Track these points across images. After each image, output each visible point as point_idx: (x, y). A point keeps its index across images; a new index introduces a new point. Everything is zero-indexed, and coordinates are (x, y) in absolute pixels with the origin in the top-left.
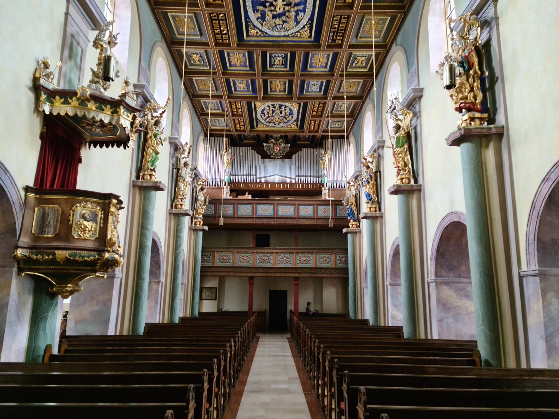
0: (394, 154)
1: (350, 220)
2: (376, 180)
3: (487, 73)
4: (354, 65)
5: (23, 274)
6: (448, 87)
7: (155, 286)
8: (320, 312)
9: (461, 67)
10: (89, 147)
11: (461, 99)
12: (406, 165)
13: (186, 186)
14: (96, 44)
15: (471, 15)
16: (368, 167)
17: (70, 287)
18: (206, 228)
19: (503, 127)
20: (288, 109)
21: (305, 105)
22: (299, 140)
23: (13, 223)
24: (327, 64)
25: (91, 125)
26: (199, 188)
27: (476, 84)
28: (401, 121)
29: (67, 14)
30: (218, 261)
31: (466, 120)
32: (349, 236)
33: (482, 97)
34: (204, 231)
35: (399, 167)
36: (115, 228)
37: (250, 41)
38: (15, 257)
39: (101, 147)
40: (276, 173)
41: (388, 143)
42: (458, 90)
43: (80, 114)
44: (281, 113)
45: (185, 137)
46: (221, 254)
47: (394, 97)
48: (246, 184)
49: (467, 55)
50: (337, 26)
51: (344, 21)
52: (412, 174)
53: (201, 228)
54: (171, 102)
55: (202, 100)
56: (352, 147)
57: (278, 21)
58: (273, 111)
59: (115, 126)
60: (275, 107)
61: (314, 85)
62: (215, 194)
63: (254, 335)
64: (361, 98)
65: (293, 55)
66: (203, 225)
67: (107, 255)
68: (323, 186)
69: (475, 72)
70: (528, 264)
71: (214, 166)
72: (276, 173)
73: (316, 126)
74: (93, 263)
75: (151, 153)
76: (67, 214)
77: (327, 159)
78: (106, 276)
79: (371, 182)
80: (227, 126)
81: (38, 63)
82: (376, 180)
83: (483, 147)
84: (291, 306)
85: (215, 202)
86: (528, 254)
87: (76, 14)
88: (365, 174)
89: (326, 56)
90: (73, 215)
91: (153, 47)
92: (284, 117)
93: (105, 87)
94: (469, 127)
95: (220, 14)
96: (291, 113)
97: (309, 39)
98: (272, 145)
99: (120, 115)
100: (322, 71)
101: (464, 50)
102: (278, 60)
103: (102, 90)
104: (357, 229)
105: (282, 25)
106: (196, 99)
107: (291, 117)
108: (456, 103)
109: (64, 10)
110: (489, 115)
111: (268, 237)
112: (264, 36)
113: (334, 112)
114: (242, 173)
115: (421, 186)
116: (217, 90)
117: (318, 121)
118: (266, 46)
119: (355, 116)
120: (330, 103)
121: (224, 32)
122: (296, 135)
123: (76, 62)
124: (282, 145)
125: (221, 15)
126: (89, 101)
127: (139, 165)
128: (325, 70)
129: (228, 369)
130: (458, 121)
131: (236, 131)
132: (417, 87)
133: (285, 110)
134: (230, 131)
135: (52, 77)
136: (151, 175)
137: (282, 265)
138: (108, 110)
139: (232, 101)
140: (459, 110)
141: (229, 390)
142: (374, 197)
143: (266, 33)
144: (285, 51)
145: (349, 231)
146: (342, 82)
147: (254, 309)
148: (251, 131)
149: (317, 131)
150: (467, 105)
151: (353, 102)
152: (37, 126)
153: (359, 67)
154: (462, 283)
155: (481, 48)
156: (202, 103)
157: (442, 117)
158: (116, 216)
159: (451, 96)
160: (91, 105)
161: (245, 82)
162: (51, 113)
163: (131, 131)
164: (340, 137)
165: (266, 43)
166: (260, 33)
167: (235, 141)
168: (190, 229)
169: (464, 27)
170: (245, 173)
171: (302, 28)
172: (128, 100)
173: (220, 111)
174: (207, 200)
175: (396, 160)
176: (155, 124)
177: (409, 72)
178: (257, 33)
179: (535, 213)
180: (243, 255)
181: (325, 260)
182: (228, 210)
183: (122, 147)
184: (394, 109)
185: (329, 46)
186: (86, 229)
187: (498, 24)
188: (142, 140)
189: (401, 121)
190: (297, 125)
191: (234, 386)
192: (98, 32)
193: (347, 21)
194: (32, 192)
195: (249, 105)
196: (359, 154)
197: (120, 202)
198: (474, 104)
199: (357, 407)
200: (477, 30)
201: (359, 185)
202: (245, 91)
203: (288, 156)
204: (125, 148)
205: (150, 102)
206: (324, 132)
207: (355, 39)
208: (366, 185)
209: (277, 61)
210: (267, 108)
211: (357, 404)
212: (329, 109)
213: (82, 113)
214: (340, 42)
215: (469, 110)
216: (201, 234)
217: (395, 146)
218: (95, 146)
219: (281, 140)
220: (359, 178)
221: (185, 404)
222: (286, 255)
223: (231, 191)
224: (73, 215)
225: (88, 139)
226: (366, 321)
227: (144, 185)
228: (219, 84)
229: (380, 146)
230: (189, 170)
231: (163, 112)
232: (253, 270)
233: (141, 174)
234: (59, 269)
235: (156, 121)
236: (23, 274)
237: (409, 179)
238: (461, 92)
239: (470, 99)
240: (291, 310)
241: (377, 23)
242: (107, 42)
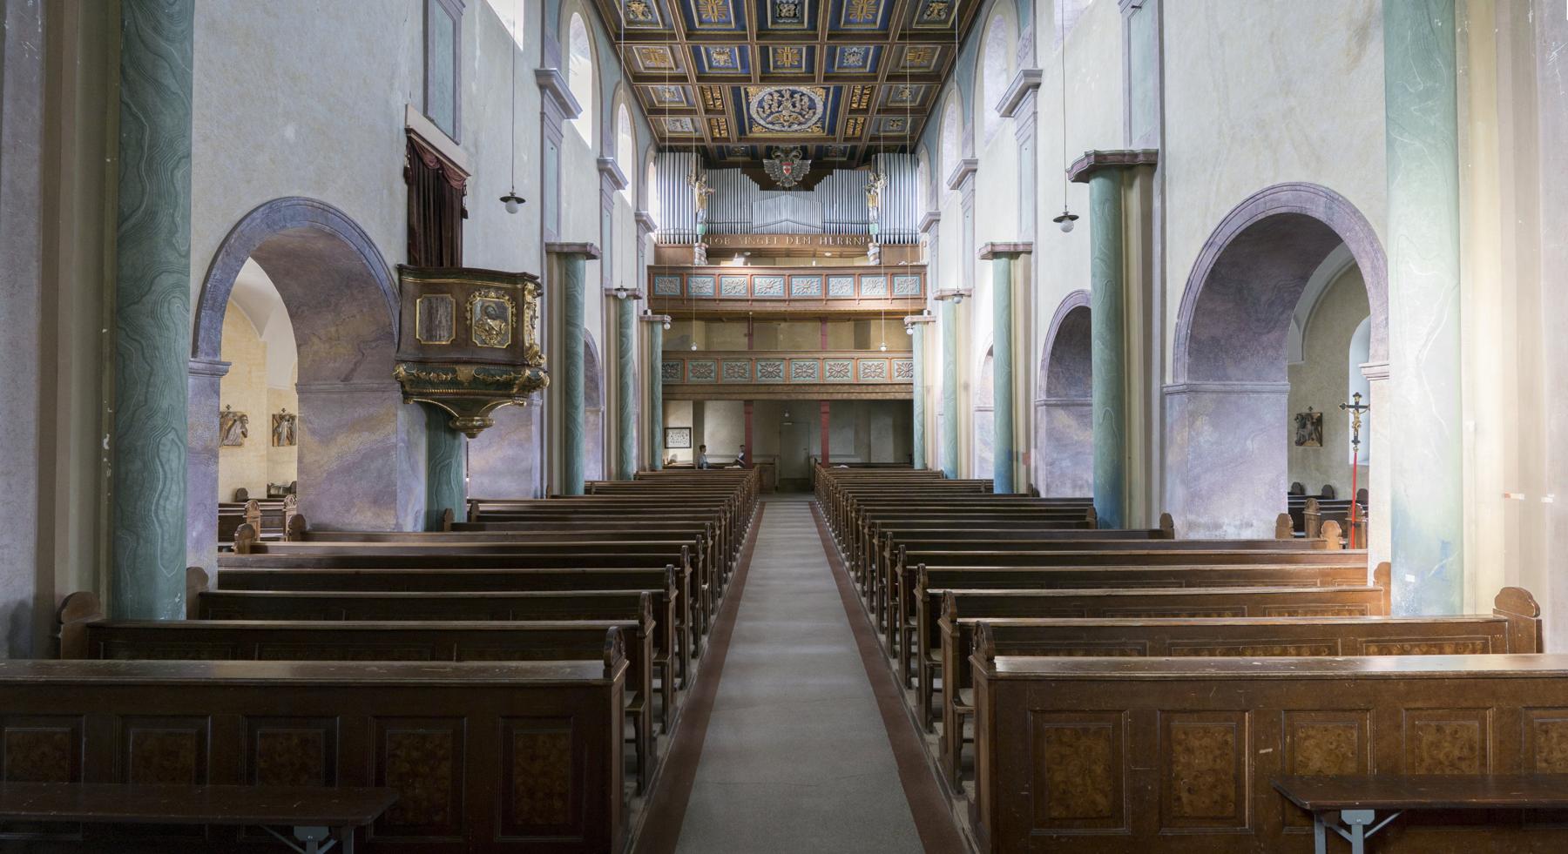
19: (1156, 153)
20: (806, 99)
21: (838, 91)
29: (543, 114)
38: (397, 377)
55: (650, 86)
58: (780, 104)
70: (1175, 376)
74: (508, 385)
86: (1176, 360)
96: (812, 106)
117: (861, 120)
124: (797, 161)
131: (714, 139)
134: (702, 140)
139: (705, 85)
148: (740, 140)
151: (923, 86)
167: (712, 159)
179: (1191, 297)
186: (492, 334)
194: (409, 274)
195: (736, 93)
196: (969, 125)
197: (538, 286)
203: (807, 184)
221: (636, 622)
228: (680, 55)
232: (751, 389)
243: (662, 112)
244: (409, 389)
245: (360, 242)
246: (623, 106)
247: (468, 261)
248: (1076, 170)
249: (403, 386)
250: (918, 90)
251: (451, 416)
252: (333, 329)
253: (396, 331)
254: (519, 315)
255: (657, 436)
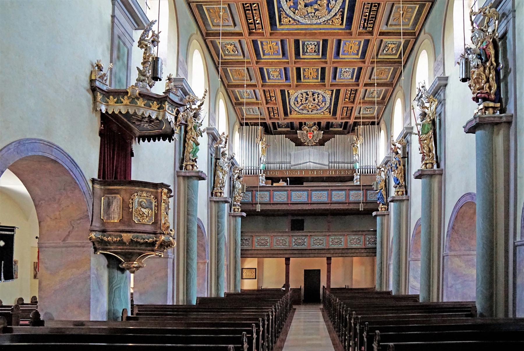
0: (420, 141)
1: (380, 203)
2: (404, 166)
3: (501, 65)
4: (385, 52)
5: (99, 253)
6: (464, 80)
7: (201, 266)
8: (350, 287)
9: (479, 59)
10: (139, 142)
11: (479, 89)
12: (430, 151)
13: (224, 175)
14: (141, 44)
15: (490, 8)
16: (397, 153)
17: (136, 264)
18: (244, 214)
19: (512, 116)
20: (320, 96)
21: (338, 91)
22: (332, 127)
23: (86, 210)
24: (358, 51)
25: (141, 121)
26: (236, 176)
27: (491, 75)
28: (427, 108)
29: (113, 16)
30: (257, 244)
31: (482, 109)
32: (378, 218)
33: (496, 88)
34: (242, 217)
35: (424, 153)
36: (167, 214)
37: (283, 29)
38: (90, 239)
39: (149, 141)
40: (310, 159)
41: (415, 131)
42: (476, 81)
43: (131, 112)
44: (314, 100)
45: (222, 128)
46: (259, 238)
47: (421, 85)
48: (280, 170)
49: (485, 47)
50: (367, 14)
51: (374, 9)
52: (435, 159)
53: (239, 215)
54: (207, 94)
55: (236, 90)
56: (383, 133)
57: (309, 9)
59: (161, 121)
60: (308, 95)
61: (346, 72)
62: (252, 182)
63: (291, 306)
64: (391, 85)
65: (325, 42)
66: (241, 211)
67: (163, 238)
68: (355, 172)
69: (492, 64)
71: (245, 153)
72: (310, 159)
73: (349, 112)
74: (153, 244)
75: (191, 145)
76: (128, 203)
77: (359, 146)
78: (162, 256)
79: (399, 168)
80: (261, 114)
81: (93, 66)
82: (404, 166)
83: (495, 134)
84: (323, 283)
85: (251, 189)
87: (122, 17)
88: (394, 160)
89: (357, 43)
90: (132, 203)
91: (187, 49)
92: (318, 104)
93: (150, 84)
94: (484, 116)
95: (254, 4)
96: (324, 101)
97: (341, 27)
98: (305, 132)
99: (166, 110)
100: (354, 58)
101: (483, 42)
102: (311, 47)
103: (148, 88)
104: (386, 213)
105: (314, 13)
106: (230, 90)
107: (323, 104)
108: (473, 93)
109: (110, 12)
110: (501, 105)
111: (302, 222)
112: (297, 24)
113: (365, 99)
114: (277, 161)
115: (442, 170)
116: (251, 80)
118: (298, 34)
119: (385, 102)
120: (361, 90)
121: (257, 22)
122: (329, 122)
123: (124, 62)
124: (315, 132)
125: (254, 5)
126: (138, 99)
127: (182, 156)
128: (357, 57)
129: (270, 329)
130: (473, 109)
132: (442, 76)
133: (318, 97)
134: (264, 119)
135: (105, 78)
136: (192, 166)
137: (316, 247)
138: (155, 105)
140: (476, 99)
141: (272, 344)
142: (401, 181)
143: (298, 21)
144: (318, 39)
145: (378, 214)
146: (373, 68)
147: (292, 286)
149: (349, 118)
150: (483, 95)
151: (384, 89)
152: (97, 124)
153: (389, 55)
154: (471, 255)
155: (497, 40)
156: (237, 93)
157: (462, 105)
158: (167, 204)
159: (470, 86)
160: (141, 103)
161: (278, 70)
162: (107, 112)
163: (176, 125)
164: (374, 123)
165: (299, 31)
166: (292, 22)
168: (230, 215)
169: (483, 20)
170: (279, 160)
171: (334, 16)
172: (171, 96)
173: (254, 100)
174: (245, 188)
175: (421, 146)
176: (194, 117)
177: (435, 60)
178: (290, 21)
180: (280, 238)
181: (353, 241)
182: (263, 197)
183: (167, 140)
184: (421, 97)
185: (360, 34)
186: (143, 217)
187: (514, 17)
188: (183, 132)
189: (427, 108)
190: (330, 112)
191: (275, 343)
192: (143, 31)
193: (377, 13)
195: (283, 92)
196: (440, 57)
197: (170, 191)
198: (488, 94)
199: (373, 345)
200: (495, 23)
201: (388, 169)
202: (279, 79)
203: (321, 143)
204: (170, 142)
205: (189, 94)
206: (356, 118)
207: (386, 26)
208: (394, 171)
209: (309, 48)
210: (300, 95)
211: (373, 343)
212: (361, 96)
213: (133, 111)
214: (371, 29)
215: (485, 99)
216: (239, 219)
217: (421, 133)
218: (144, 141)
219: (314, 127)
220: (389, 164)
222: (320, 238)
223: (267, 178)
224: (132, 203)
225: (138, 134)
226: (389, 293)
227: (188, 174)
229: (407, 133)
230: (226, 160)
231: (202, 104)
233: (184, 165)
234: (126, 249)
235: (195, 114)
236: (99, 253)
237: (432, 163)
238: (478, 83)
239: (486, 90)
240: (324, 287)
241: (405, 11)
242: (150, 41)
243: (242, 104)
244: (99, 245)
245: (71, 165)
246: (237, 132)
247: (134, 177)
248: (469, 127)
249: (94, 244)
250: (381, 91)
251: (120, 262)
252: (57, 213)
253: (90, 215)
254: (158, 206)
255: (237, 273)
